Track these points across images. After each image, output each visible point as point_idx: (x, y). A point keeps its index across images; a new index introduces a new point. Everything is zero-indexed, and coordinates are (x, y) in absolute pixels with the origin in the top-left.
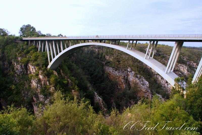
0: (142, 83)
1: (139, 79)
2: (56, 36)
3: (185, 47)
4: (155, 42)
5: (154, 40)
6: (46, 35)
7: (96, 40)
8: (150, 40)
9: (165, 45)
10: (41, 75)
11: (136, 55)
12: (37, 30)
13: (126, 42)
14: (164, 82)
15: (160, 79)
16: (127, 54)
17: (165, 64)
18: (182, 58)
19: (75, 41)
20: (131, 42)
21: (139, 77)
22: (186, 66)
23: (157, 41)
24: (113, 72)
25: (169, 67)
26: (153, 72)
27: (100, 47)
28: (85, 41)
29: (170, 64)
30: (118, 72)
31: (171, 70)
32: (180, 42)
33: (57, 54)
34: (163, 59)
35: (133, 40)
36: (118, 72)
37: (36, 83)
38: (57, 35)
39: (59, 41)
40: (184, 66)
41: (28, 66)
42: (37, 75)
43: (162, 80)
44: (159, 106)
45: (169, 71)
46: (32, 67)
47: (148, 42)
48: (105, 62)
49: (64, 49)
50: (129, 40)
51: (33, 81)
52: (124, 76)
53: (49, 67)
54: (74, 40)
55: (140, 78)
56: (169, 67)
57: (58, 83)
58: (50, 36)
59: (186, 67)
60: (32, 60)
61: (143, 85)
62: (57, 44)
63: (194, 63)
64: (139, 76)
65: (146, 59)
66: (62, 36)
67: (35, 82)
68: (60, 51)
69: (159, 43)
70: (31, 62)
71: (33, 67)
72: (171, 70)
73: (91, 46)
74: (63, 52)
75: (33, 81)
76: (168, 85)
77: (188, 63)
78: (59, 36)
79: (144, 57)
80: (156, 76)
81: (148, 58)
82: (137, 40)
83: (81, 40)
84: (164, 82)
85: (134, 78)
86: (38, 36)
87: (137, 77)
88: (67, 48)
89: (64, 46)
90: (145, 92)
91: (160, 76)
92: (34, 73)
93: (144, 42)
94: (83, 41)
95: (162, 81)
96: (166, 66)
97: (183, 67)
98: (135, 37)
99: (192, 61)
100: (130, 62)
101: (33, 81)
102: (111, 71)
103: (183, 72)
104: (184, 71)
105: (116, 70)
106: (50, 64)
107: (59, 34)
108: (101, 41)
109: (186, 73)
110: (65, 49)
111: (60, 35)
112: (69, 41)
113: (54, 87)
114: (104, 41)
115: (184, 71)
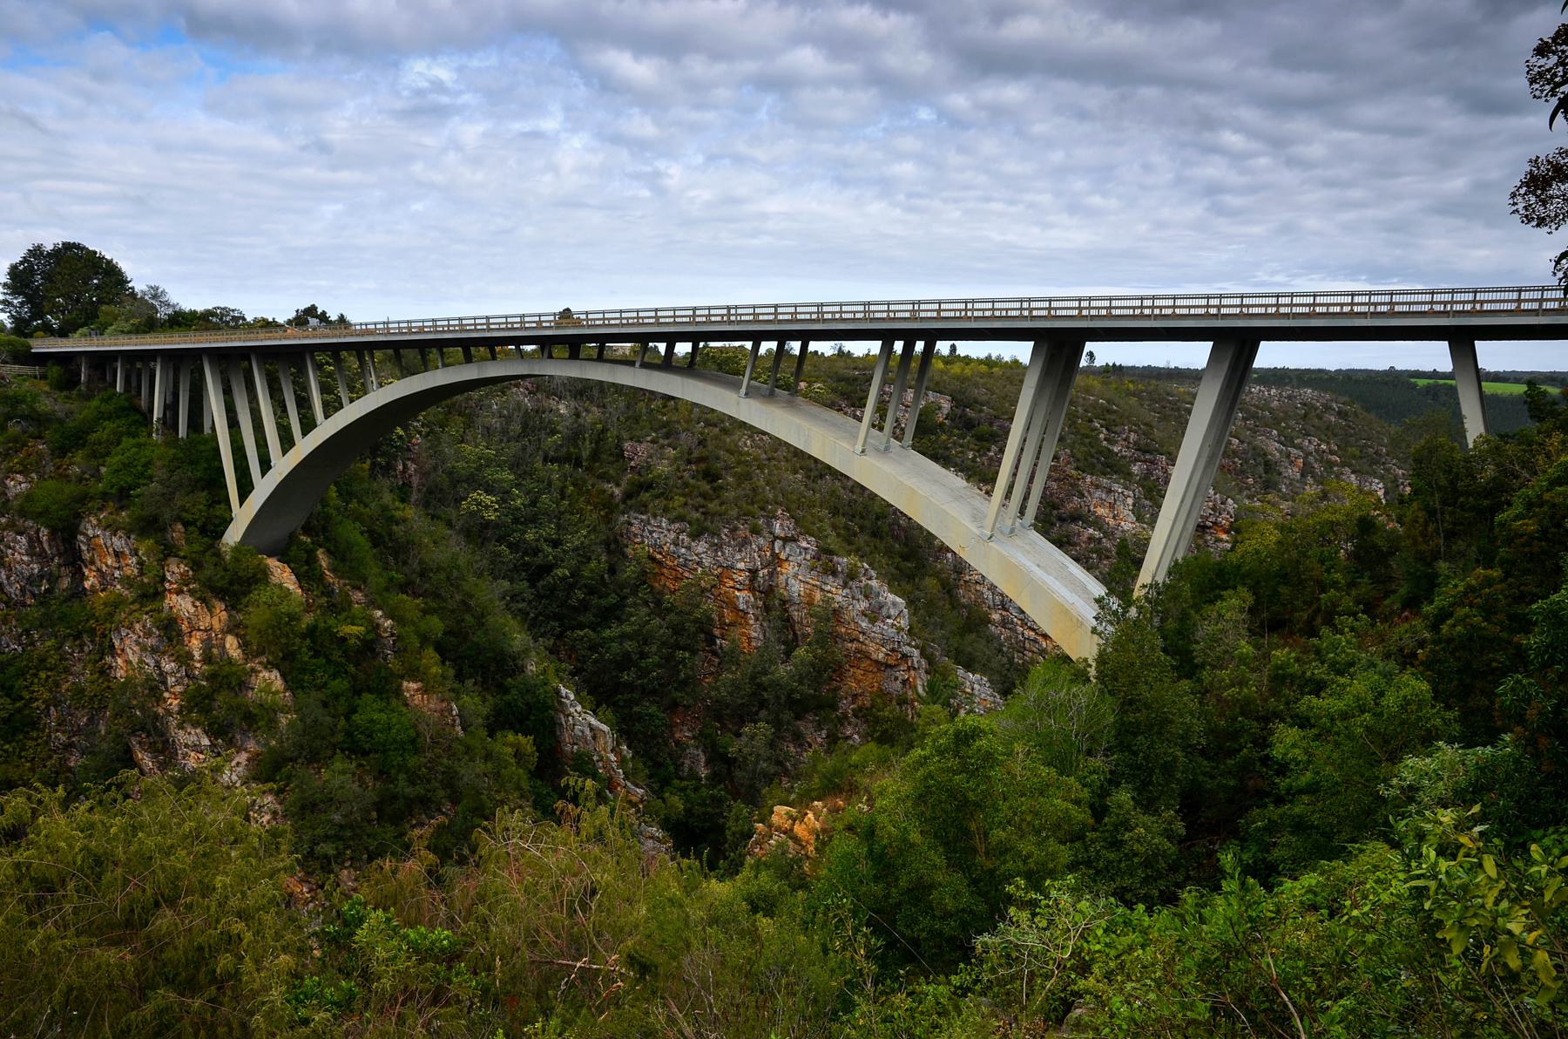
4: (920, 346)
23: (931, 336)
27: (583, 390)
49: (331, 408)
52: (750, 571)
69: (943, 347)
74: (327, 428)
77: (1135, 469)
103: (1112, 522)
111: (311, 311)
114: (662, 347)
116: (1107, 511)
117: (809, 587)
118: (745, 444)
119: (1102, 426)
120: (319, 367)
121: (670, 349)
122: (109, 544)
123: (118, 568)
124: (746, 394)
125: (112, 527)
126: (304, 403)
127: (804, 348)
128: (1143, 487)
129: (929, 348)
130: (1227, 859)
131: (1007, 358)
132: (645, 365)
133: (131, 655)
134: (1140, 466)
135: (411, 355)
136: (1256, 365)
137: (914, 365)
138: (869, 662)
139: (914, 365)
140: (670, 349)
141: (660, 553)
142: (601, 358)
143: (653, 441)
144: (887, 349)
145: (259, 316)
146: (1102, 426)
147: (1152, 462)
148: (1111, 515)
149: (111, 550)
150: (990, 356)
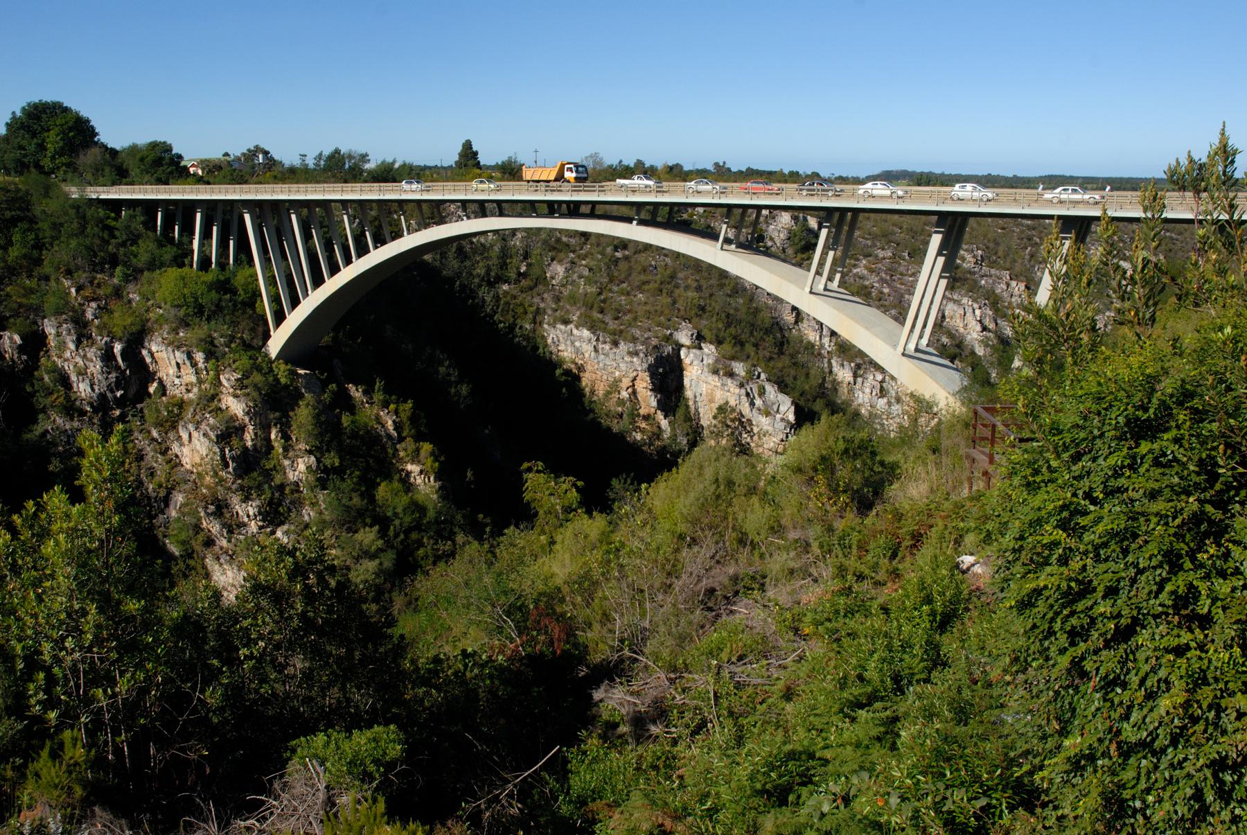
1: (741, 386)
10: (236, 396)
11: (746, 264)
16: (660, 250)
17: (900, 319)
21: (743, 374)
22: (974, 300)
25: (913, 326)
26: (809, 342)
29: (930, 308)
31: (921, 337)
37: (210, 440)
40: (965, 300)
42: (210, 399)
45: (912, 346)
46: (178, 354)
49: (334, 270)
53: (275, 344)
55: (751, 376)
56: (913, 326)
57: (283, 561)
58: (272, 170)
63: (1014, 283)
64: (739, 368)
65: (811, 292)
67: (205, 435)
71: (180, 356)
72: (921, 337)
75: (195, 434)
79: (803, 289)
81: (821, 287)
85: (714, 380)
87: (731, 374)
88: (359, 256)
102: (587, 349)
103: (962, 330)
106: (275, 344)
109: (975, 335)
123: (179, 377)
124: (409, 233)
148: (961, 325)
149: (173, 363)
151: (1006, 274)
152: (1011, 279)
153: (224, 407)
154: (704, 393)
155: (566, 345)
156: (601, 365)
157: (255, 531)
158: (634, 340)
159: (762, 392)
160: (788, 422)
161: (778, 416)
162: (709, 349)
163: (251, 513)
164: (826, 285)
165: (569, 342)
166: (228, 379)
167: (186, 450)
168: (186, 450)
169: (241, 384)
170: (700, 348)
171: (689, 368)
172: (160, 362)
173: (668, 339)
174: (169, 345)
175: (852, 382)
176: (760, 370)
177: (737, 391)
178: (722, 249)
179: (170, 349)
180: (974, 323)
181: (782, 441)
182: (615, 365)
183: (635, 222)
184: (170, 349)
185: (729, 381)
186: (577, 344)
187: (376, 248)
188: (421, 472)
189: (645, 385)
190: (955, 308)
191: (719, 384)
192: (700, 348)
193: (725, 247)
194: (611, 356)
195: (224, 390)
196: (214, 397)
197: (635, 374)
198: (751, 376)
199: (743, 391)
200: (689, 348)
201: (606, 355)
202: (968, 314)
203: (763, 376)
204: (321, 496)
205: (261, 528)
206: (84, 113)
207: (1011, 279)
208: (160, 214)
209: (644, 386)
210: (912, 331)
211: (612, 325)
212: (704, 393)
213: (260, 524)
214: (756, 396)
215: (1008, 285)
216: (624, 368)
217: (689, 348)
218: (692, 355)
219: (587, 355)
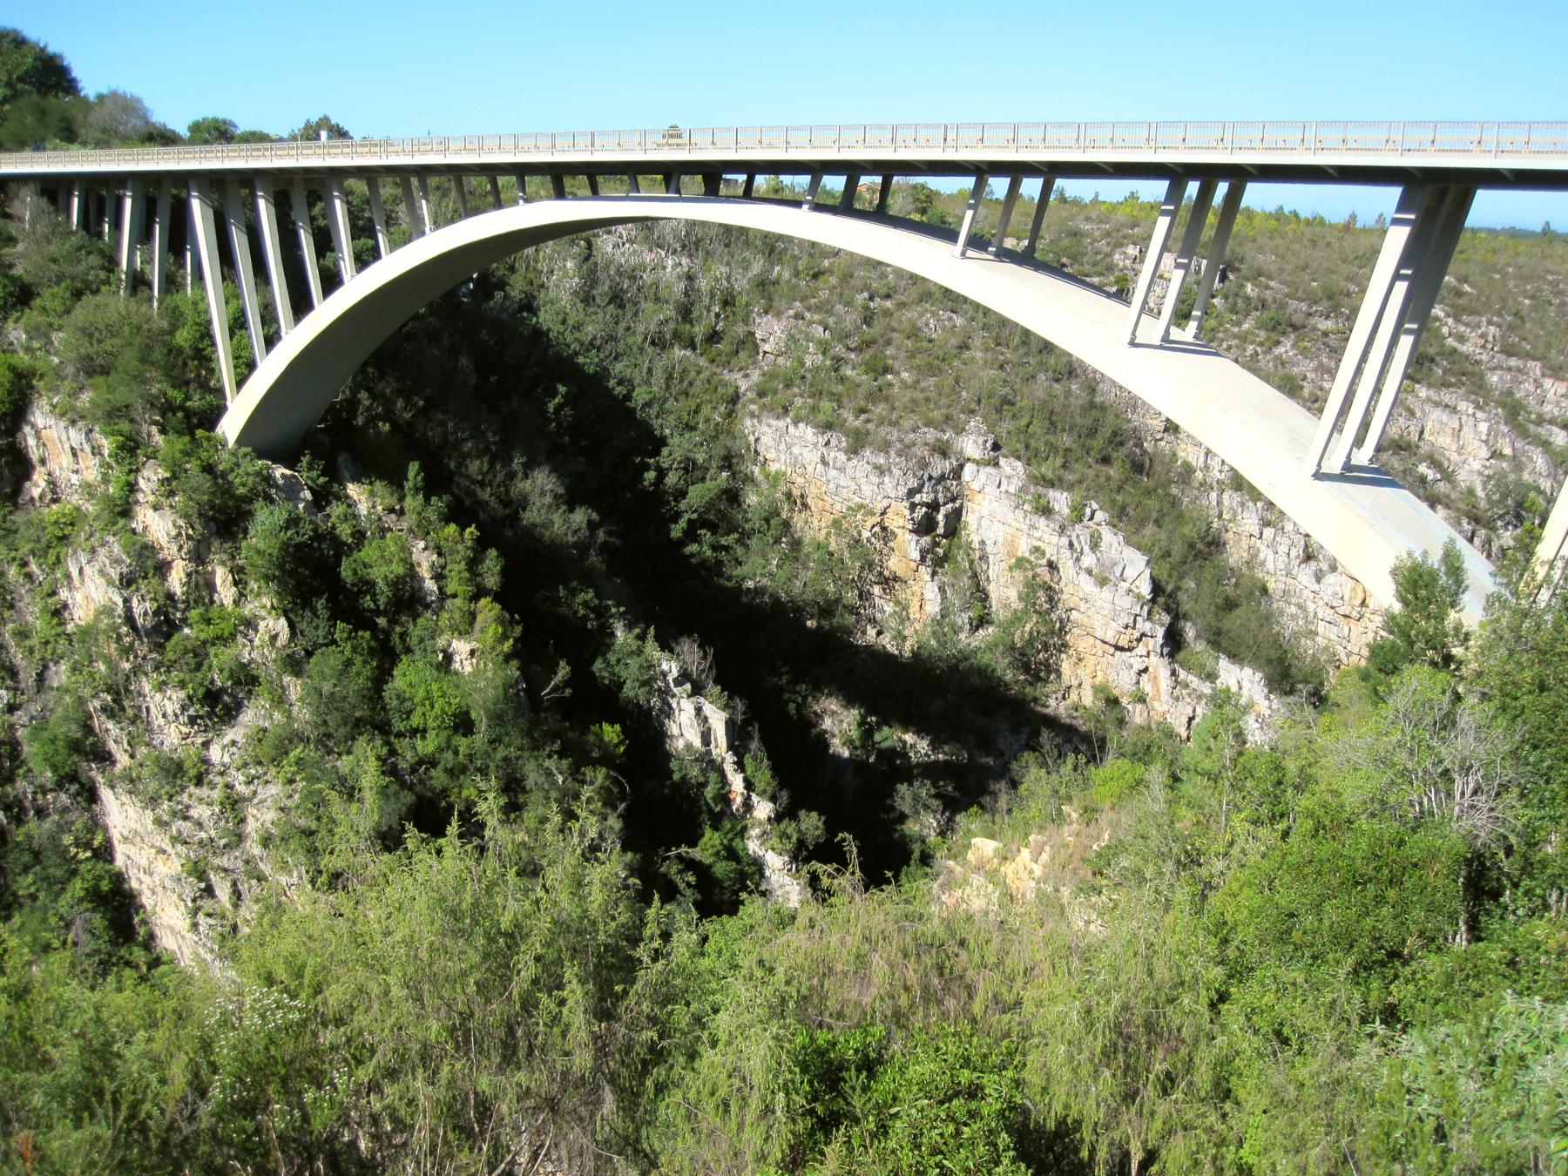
0: (1088, 560)
2: (281, 140)
3: (1474, 231)
4: (1222, 188)
5: (1209, 174)
6: (184, 132)
7: (671, 174)
8: (1177, 174)
9: (1296, 215)
10: (156, 508)
12: (92, 80)
13: (1088, 198)
14: (1283, 549)
15: (1249, 521)
16: (952, 300)
18: (1445, 330)
19: (502, 180)
20: (999, 186)
21: (1066, 511)
23: (1240, 175)
24: (824, 462)
27: (694, 239)
28: (568, 182)
30: (877, 467)
31: (1359, 441)
32: (1443, 194)
33: (301, 305)
34: (1278, 343)
35: (1016, 171)
36: (877, 467)
37: (110, 583)
38: (298, 125)
39: (317, 183)
41: (33, 426)
43: (1269, 532)
44: (182, 452)
46: (72, 432)
47: (1156, 189)
48: (755, 376)
49: (365, 259)
50: (982, 170)
51: (81, 571)
53: (231, 426)
54: (457, 172)
55: (1078, 515)
59: (1480, 415)
60: (58, 374)
61: (1102, 582)
62: (262, 203)
64: (1060, 500)
66: (339, 133)
67: (102, 572)
68: (331, 282)
69: (1257, 196)
70: (56, 390)
71: (76, 437)
72: (1359, 441)
73: (620, 228)
74: (357, 286)
76: (1318, 580)
77: (1494, 379)
78: (310, 133)
80: (1214, 495)
82: (1052, 171)
83: (522, 171)
84: (1283, 549)
86: (107, 139)
87: (1046, 511)
89: (362, 229)
90: (1118, 648)
91: (1255, 495)
92: (87, 487)
93: (1113, 190)
94: (694, 183)
95: (1272, 545)
96: (1321, 411)
97: (1454, 410)
98: (1256, 144)
99: (1531, 364)
100: (980, 369)
101: (81, 571)
102: (811, 457)
103: (1454, 457)
104: (1460, 450)
105: (853, 451)
106: (231, 426)
107: (314, 119)
108: (711, 176)
110: (375, 255)
111: (324, 122)
112: (406, 186)
113: (283, 622)
114: (742, 178)
115: (1460, 450)
116: (1448, 440)
117: (1011, 530)
118: (927, 325)
119: (1448, 315)
120: (347, 194)
121: (851, 186)
122: (64, 438)
123: (77, 472)
125: (73, 417)
126: (325, 242)
127: (1046, 190)
128: (1504, 406)
129: (1234, 197)
130: (443, 804)
131: (1305, 214)
132: (819, 207)
133: (93, 589)
134: (1501, 378)
135: (474, 182)
136: (1243, 205)
137: (1211, 219)
138: (1091, 640)
139: (1211, 219)
140: (851, 186)
141: (803, 475)
142: (748, 195)
143: (798, 316)
144: (1175, 194)
145: (210, 115)
146: (1448, 315)
147: (1519, 370)
148: (1454, 447)
149: (67, 447)
150: (1281, 208)
151: (1535, 367)
152: (1543, 375)
153: (140, 529)
154: (1000, 540)
155: (778, 450)
156: (832, 486)
157: (176, 741)
158: (885, 447)
159: (1095, 545)
160: (1138, 597)
161: (1125, 585)
162: (1013, 469)
163: (170, 712)
164: (1167, 332)
165: (782, 447)
166: (150, 478)
167: (79, 597)
168: (79, 597)
169: (169, 487)
170: (997, 465)
171: (978, 498)
172: (49, 446)
173: (943, 451)
174: (63, 415)
175: (1257, 533)
176: (1095, 506)
177: (1055, 539)
178: (963, 254)
179: (62, 424)
180: (1477, 444)
181: (1127, 627)
182: (854, 487)
183: (805, 207)
184: (62, 424)
185: (1042, 522)
186: (796, 450)
187: (392, 250)
188: (472, 653)
189: (901, 522)
190: (1445, 418)
191: (1025, 527)
192: (997, 465)
193: (970, 253)
194: (849, 471)
195: (140, 497)
196: (126, 512)
197: (885, 503)
198: (1078, 515)
199: (1065, 541)
200: (978, 463)
201: (842, 470)
202: (1465, 429)
203: (1099, 516)
204: (295, 688)
205: (186, 737)
206: (53, 49)
207: (1543, 375)
208: (76, 200)
209: (900, 520)
210: (1338, 427)
211: (853, 422)
212: (1000, 540)
213: (185, 730)
214: (1086, 549)
215: (1538, 385)
216: (868, 494)
217: (978, 463)
218: (982, 476)
219: (810, 469)
